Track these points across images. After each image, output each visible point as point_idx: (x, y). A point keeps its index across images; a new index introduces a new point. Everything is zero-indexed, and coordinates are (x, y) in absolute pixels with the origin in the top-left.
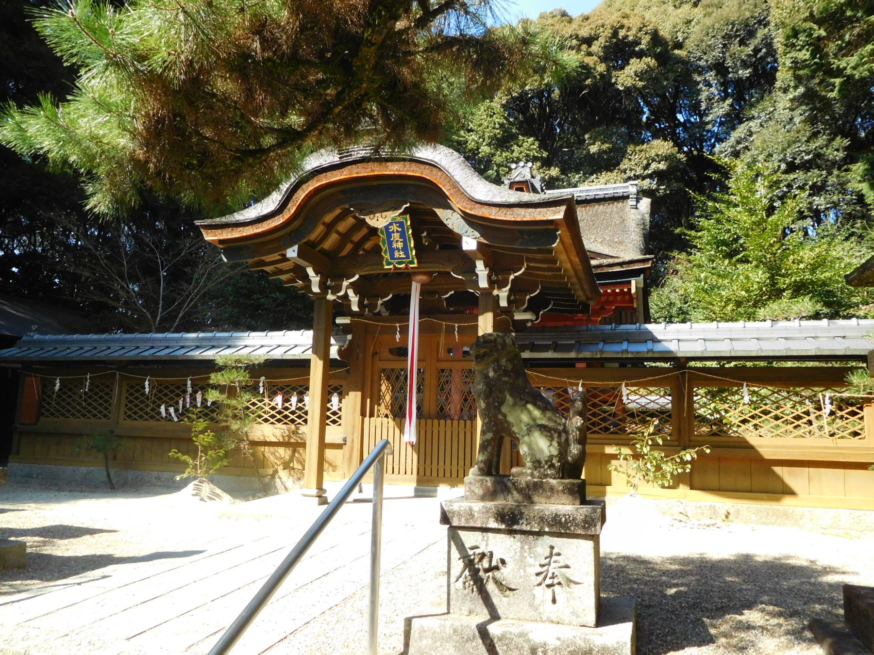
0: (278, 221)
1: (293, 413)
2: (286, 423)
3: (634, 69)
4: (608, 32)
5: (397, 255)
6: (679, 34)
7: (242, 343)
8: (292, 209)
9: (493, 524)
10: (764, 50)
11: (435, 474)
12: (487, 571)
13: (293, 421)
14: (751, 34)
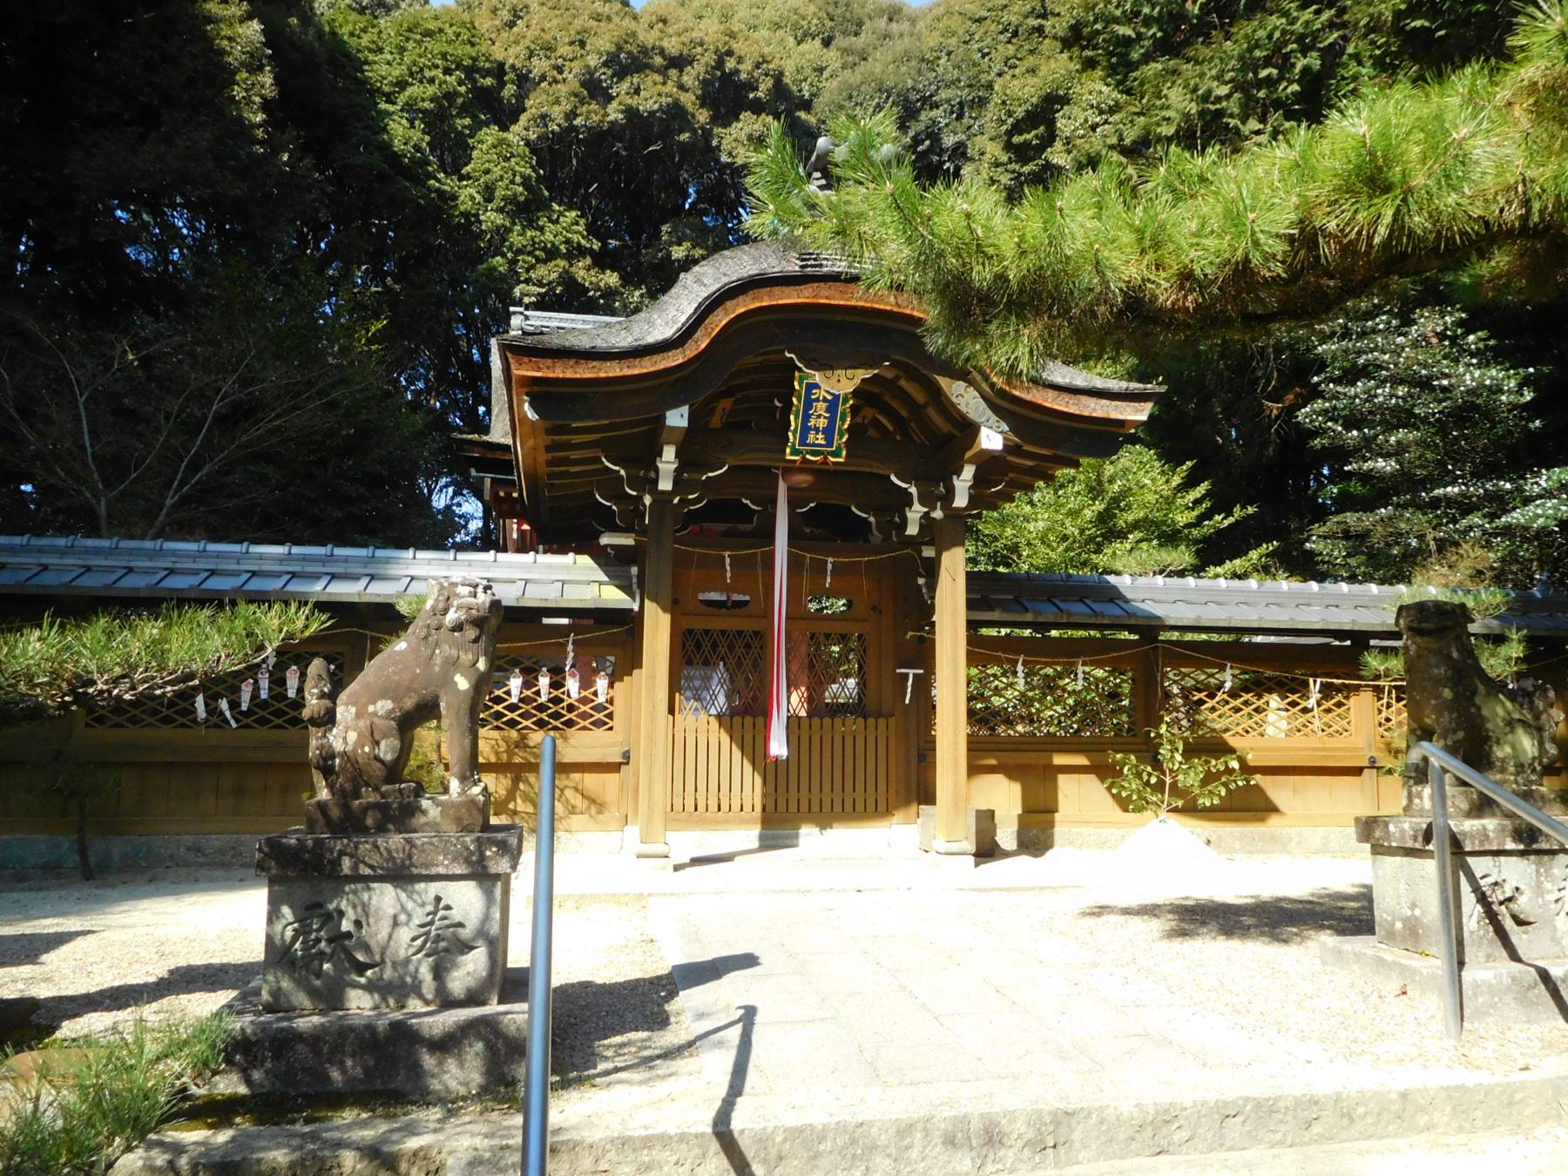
0: (675, 359)
2: (498, 728)
3: (747, 130)
4: (710, 58)
5: (811, 437)
6: (806, 86)
7: (394, 570)
8: (701, 342)
9: (1510, 845)
10: (927, 143)
11: (793, 808)
12: (1501, 903)
13: (512, 724)
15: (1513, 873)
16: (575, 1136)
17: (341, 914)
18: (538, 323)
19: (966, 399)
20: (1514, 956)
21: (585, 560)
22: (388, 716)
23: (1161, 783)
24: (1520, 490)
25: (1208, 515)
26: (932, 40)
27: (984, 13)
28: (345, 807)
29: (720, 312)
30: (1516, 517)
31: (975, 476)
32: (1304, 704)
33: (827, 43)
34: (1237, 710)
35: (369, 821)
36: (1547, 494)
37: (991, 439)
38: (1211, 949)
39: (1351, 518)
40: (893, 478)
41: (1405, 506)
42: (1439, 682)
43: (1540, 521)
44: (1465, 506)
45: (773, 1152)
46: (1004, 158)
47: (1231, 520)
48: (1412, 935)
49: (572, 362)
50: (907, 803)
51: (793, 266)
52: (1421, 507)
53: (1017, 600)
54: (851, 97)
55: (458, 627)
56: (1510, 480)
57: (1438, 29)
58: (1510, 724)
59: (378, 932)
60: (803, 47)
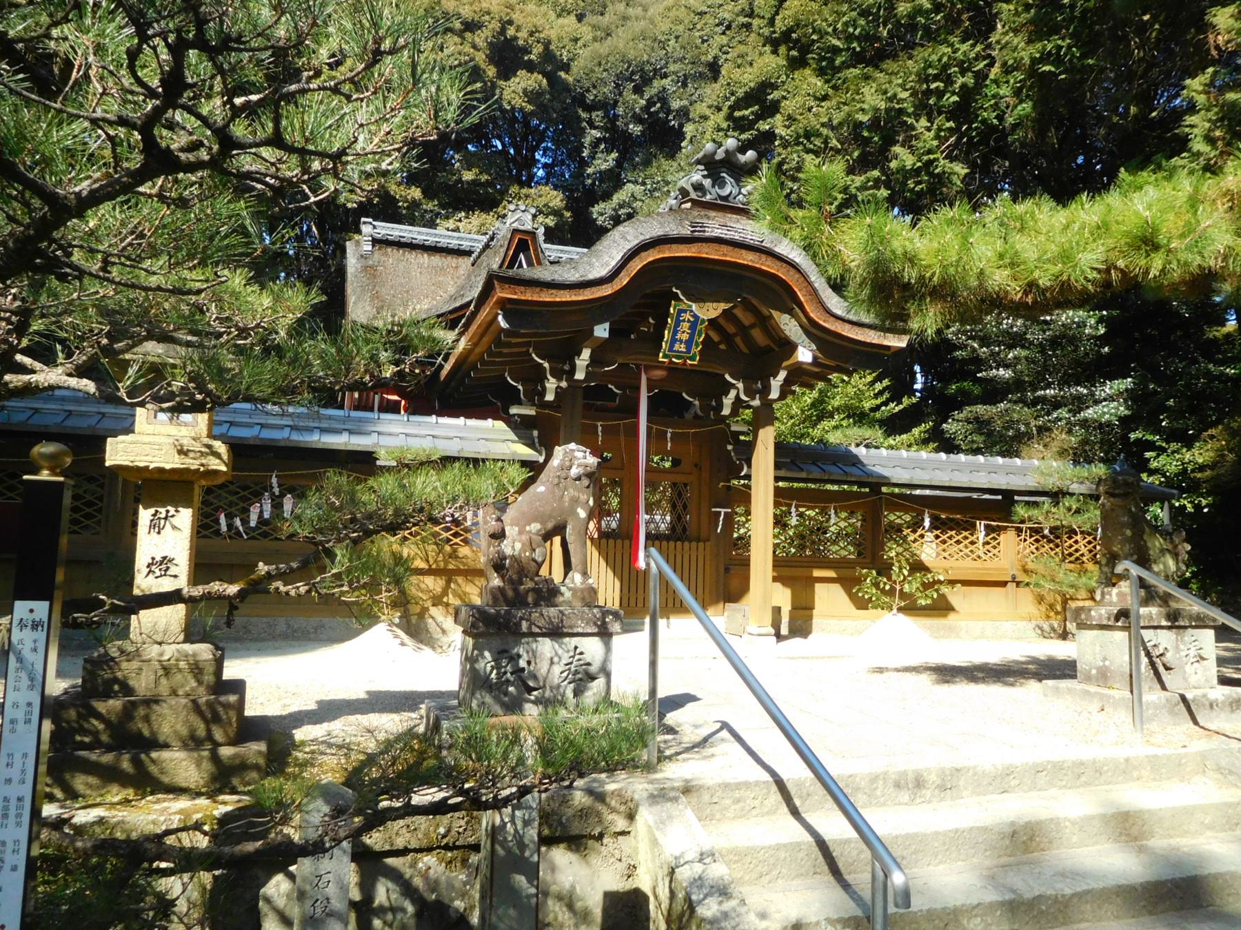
0: (606, 290)
1: (447, 529)
3: (523, 85)
4: (496, 25)
5: (676, 347)
8: (624, 280)
9: (1164, 623)
10: (658, 105)
11: (640, 605)
14: (647, 81)
15: (1163, 640)
16: (701, 783)
17: (519, 656)
18: (383, 232)
19: (789, 326)
20: (1164, 688)
21: (500, 424)
22: (537, 534)
23: (893, 590)
24: (1093, 395)
25: (885, 404)
26: (665, 26)
27: (705, 9)
28: (516, 590)
29: (637, 260)
30: (1089, 413)
31: (785, 380)
32: (971, 538)
33: (580, 18)
34: (958, 542)
35: (530, 599)
36: (1111, 398)
37: (805, 355)
38: (963, 690)
39: (980, 409)
40: (727, 377)
41: (1016, 402)
42: (1124, 525)
43: (1107, 416)
44: (1056, 404)
45: (805, 791)
46: (725, 125)
47: (901, 407)
48: (1103, 677)
49: (538, 289)
50: (716, 602)
51: (686, 231)
52: (1022, 400)
53: (793, 462)
54: (600, 64)
55: (579, 478)
56: (1085, 387)
57: (1060, 74)
58: (1163, 551)
59: (542, 668)
60: (561, 21)
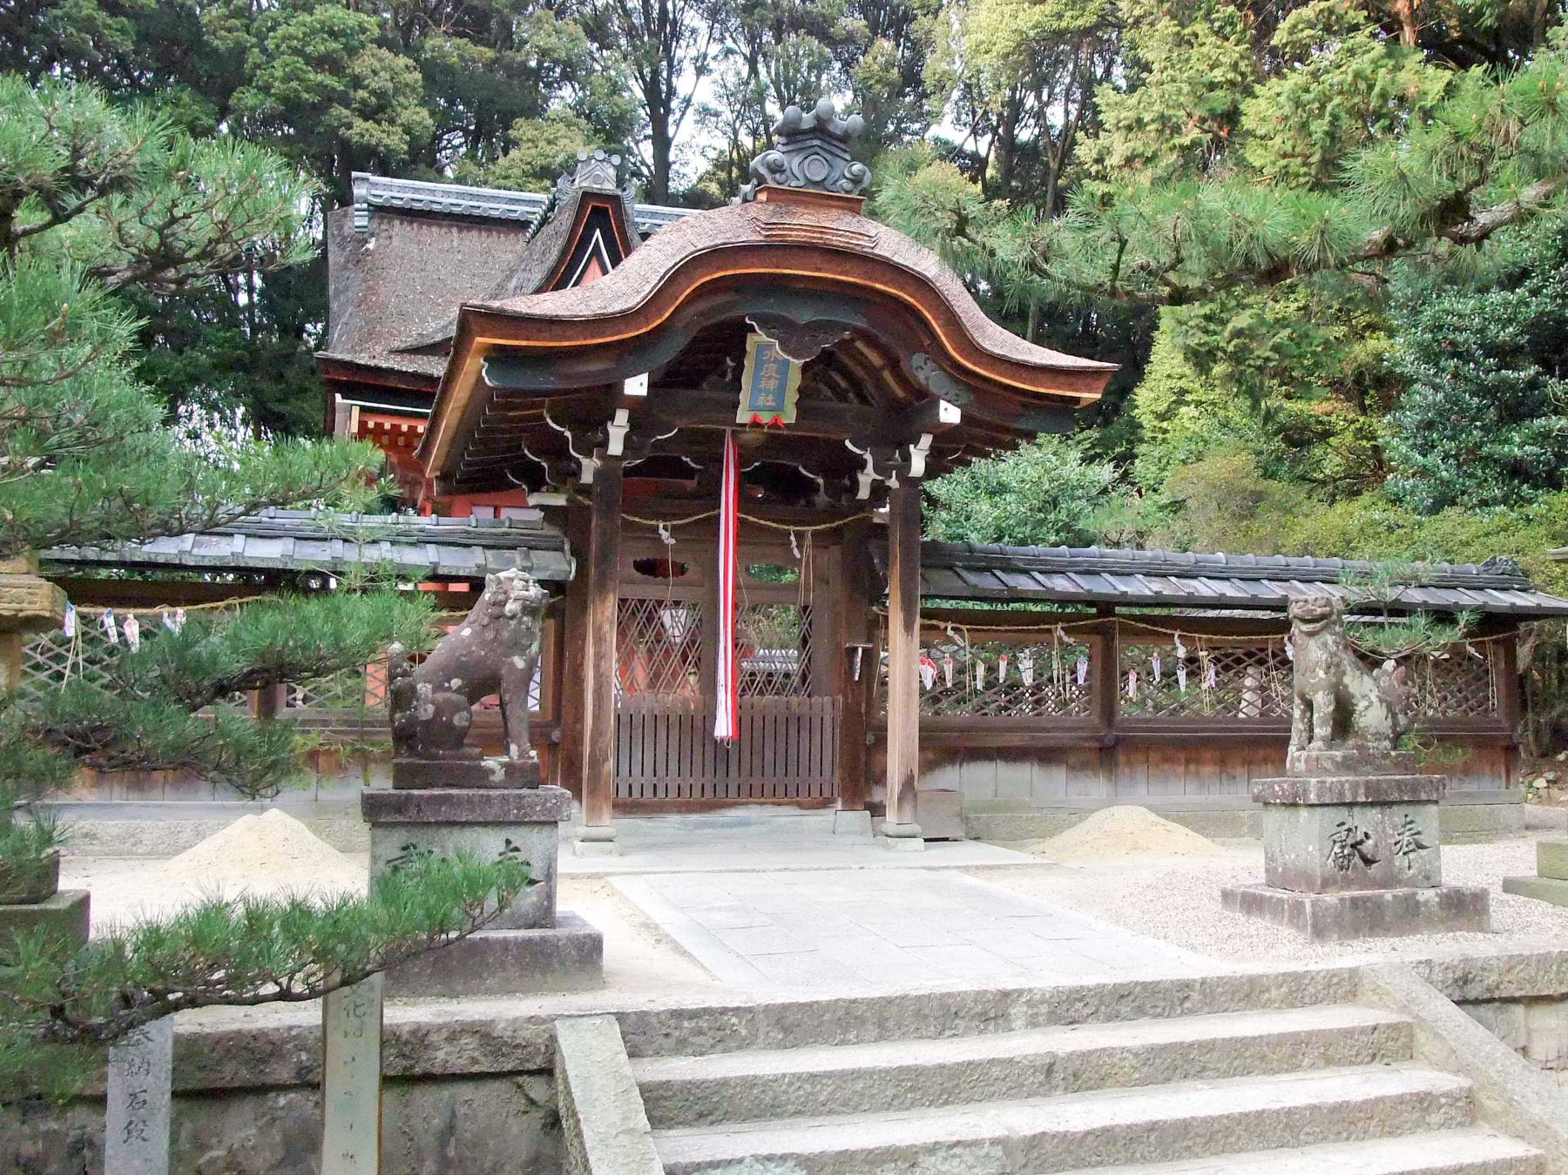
18: (387, 194)
19: (925, 372)
31: (932, 447)
40: (847, 443)
